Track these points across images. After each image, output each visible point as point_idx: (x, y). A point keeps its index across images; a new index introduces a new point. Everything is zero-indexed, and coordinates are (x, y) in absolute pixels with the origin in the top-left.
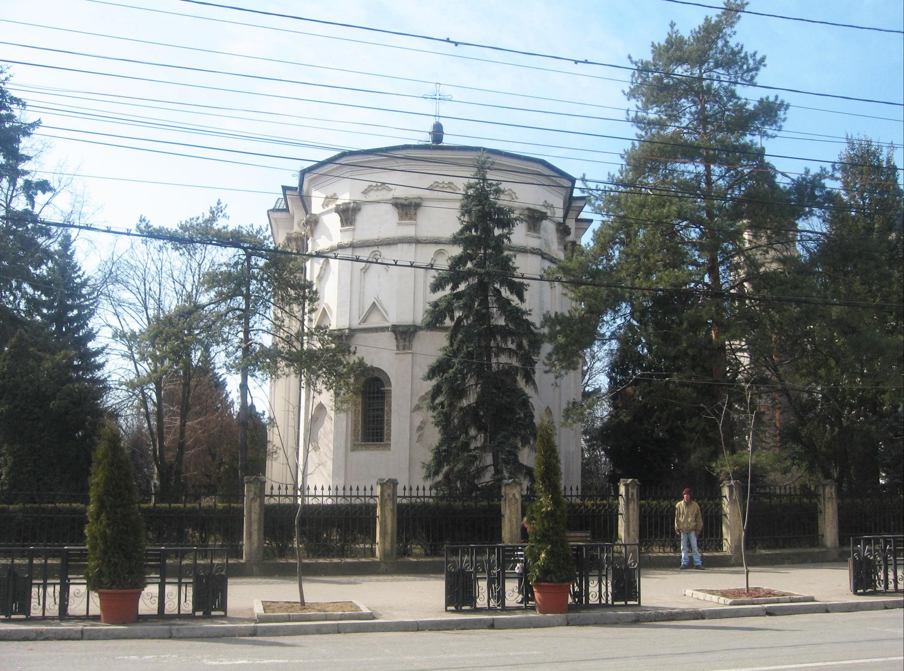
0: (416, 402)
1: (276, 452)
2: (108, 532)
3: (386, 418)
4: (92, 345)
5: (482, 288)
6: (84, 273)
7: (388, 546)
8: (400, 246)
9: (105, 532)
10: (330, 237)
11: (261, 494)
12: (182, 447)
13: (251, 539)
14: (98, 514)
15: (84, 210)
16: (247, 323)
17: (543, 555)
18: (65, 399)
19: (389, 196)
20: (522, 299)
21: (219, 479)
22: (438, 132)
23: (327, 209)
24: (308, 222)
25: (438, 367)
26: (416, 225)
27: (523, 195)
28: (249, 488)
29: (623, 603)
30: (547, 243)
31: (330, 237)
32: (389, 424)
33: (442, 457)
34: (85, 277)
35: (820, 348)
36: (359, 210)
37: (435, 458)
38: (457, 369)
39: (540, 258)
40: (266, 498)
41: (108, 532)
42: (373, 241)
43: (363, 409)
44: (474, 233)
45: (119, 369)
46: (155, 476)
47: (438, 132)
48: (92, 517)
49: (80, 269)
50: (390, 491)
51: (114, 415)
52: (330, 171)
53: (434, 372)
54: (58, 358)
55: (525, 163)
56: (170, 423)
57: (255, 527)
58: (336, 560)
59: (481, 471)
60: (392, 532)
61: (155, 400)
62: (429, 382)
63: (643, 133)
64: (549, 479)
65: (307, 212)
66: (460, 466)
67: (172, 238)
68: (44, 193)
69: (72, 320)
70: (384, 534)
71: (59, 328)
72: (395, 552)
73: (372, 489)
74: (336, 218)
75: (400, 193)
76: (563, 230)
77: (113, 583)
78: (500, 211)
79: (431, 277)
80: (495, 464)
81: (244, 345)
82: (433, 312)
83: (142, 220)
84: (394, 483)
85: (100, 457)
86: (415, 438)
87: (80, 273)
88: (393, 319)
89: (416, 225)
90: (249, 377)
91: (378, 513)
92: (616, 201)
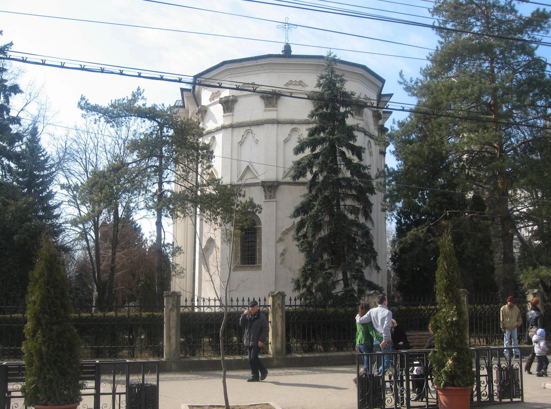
0: (279, 236)
1: (182, 272)
2: (44, 349)
3: (258, 248)
4: (51, 203)
5: (332, 152)
6: (46, 154)
7: (279, 345)
8: (266, 125)
9: (40, 349)
10: (215, 121)
11: (177, 305)
12: (113, 270)
13: (170, 340)
14: (35, 332)
15: (47, 114)
16: (161, 176)
17: (450, 362)
18: (24, 233)
20: (360, 158)
21: (138, 292)
22: (287, 49)
23: (213, 102)
24: (199, 112)
25: (301, 208)
26: (277, 110)
27: (353, 87)
28: (167, 300)
29: (509, 400)
30: (367, 125)
31: (215, 121)
32: (260, 252)
33: (308, 273)
34: (47, 156)
36: (237, 101)
37: (303, 275)
38: (317, 209)
39: (363, 134)
40: (182, 309)
41: (44, 349)
42: (246, 122)
43: (241, 241)
44: (325, 110)
45: (67, 210)
46: (95, 290)
47: (287, 49)
48: (29, 335)
49: (43, 151)
50: (279, 302)
51: (67, 250)
52: (214, 76)
53: (298, 212)
54: (20, 203)
55: (352, 67)
56: (105, 254)
57: (173, 332)
58: (238, 357)
59: (335, 283)
60: (282, 334)
61: (94, 238)
62: (294, 219)
63: (443, 40)
64: (452, 292)
65: (198, 106)
66: (320, 280)
67: (104, 112)
68: (15, 94)
69: (38, 185)
70: (275, 335)
71: (29, 191)
72: (285, 350)
73: (265, 300)
74: (220, 107)
76: (378, 117)
77: (49, 399)
78: (345, 94)
80: (345, 279)
81: (158, 193)
82: (298, 168)
83: (83, 98)
84: (282, 295)
85: (37, 275)
86: (279, 261)
87: (44, 153)
88: (262, 178)
89: (277, 110)
90: (163, 217)
91: (270, 318)
92: (427, 87)
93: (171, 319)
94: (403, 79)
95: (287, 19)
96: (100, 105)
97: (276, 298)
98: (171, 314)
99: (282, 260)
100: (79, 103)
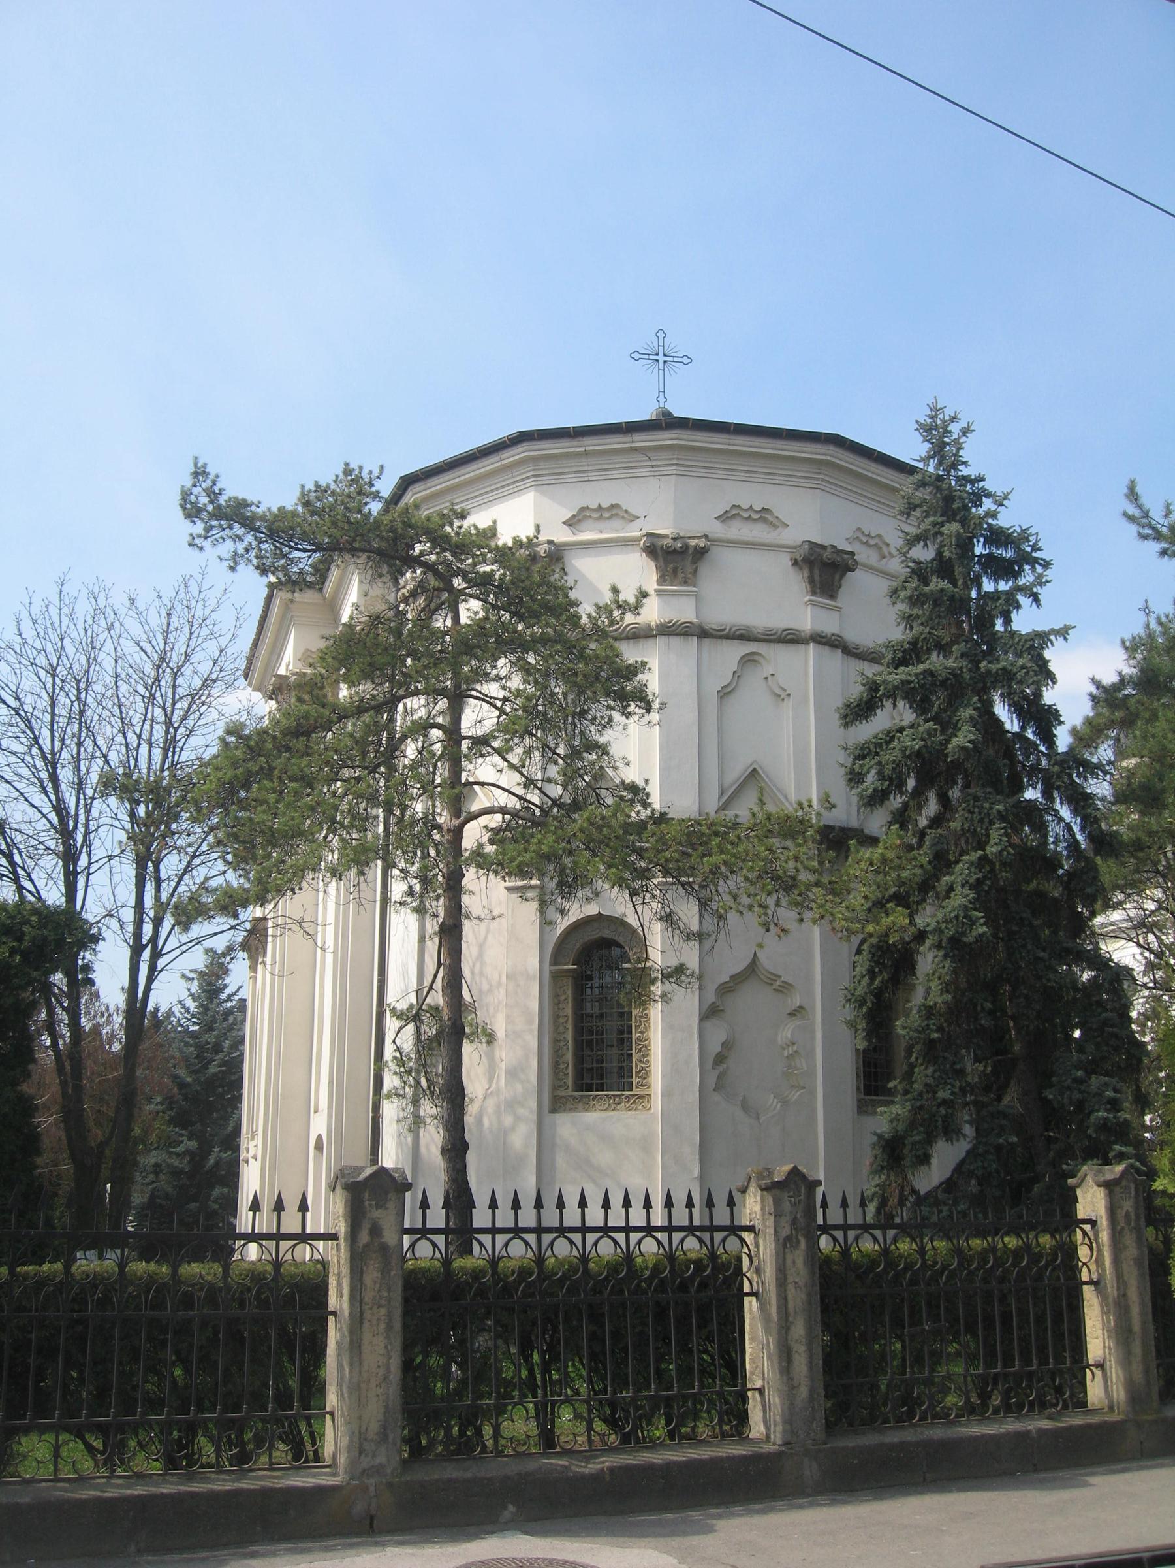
0: (711, 997)
19: (634, 531)
35: (425, 1017)
75: (664, 526)
79: (849, 680)
83: (199, 473)
93: (790, 1279)
94: (1140, 507)
95: (661, 334)
96: (326, 479)
97: (1117, 1190)
98: (789, 1258)
99: (719, 1078)
100: (185, 495)
